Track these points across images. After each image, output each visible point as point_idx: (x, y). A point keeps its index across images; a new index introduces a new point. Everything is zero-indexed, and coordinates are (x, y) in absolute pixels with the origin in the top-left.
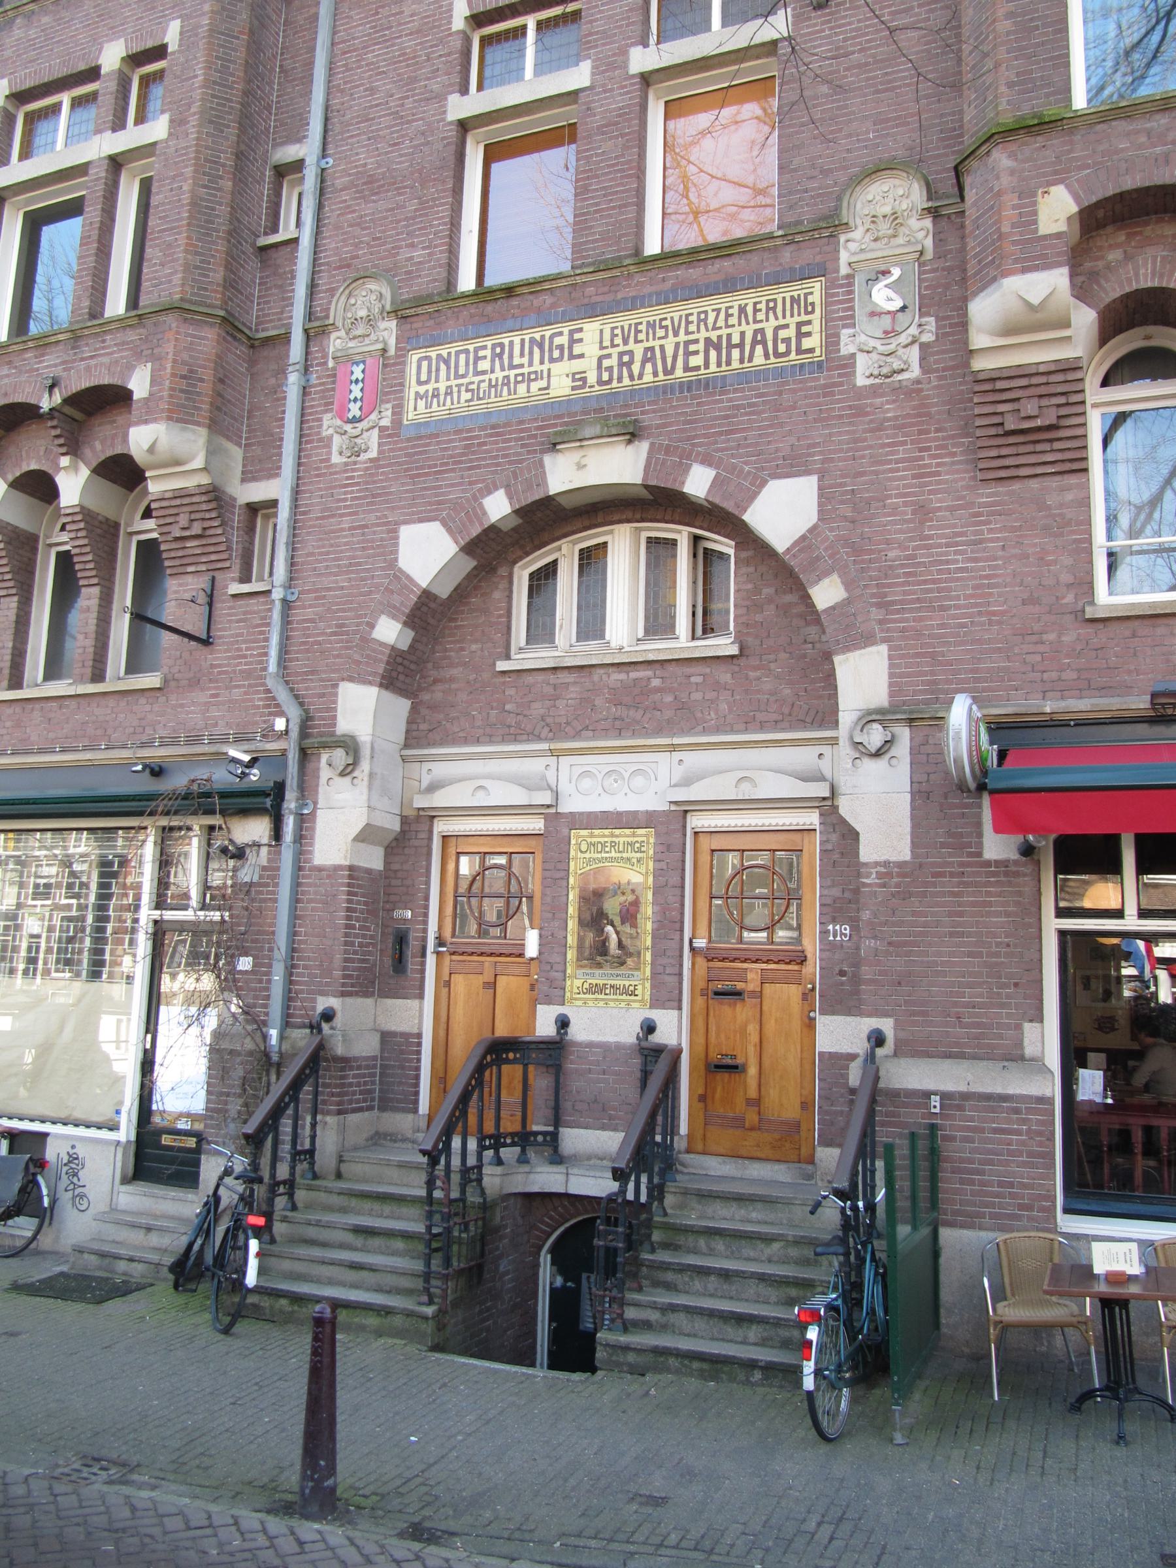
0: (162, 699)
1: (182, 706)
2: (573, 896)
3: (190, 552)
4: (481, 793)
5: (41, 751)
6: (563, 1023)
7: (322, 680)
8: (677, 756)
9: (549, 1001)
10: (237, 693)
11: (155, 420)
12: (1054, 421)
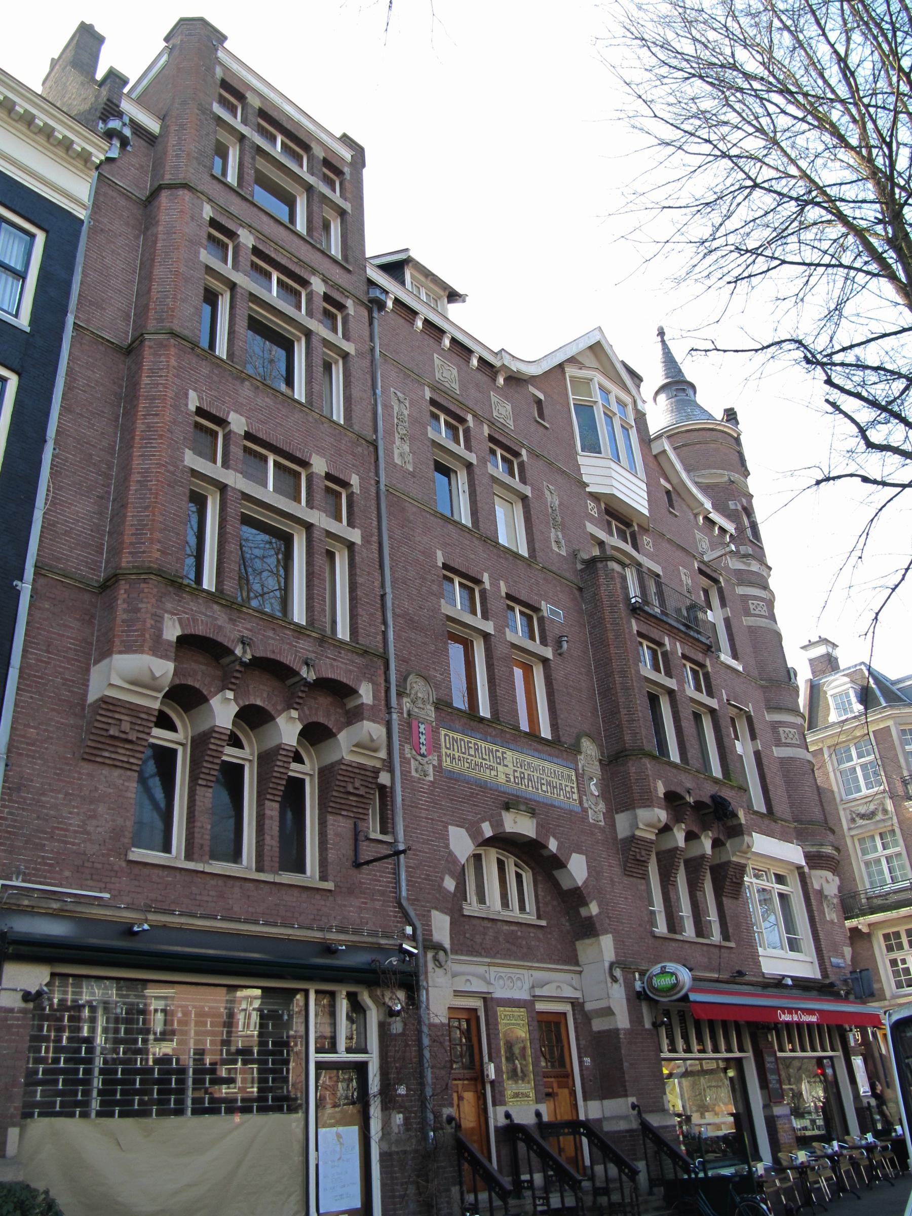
0: (331, 898)
1: (345, 906)
2: (502, 1043)
3: (349, 803)
4: (468, 983)
5: (246, 921)
6: (508, 1116)
7: (423, 906)
8: (531, 972)
9: (501, 1105)
10: (378, 905)
11: (378, 723)
12: (134, 739)
